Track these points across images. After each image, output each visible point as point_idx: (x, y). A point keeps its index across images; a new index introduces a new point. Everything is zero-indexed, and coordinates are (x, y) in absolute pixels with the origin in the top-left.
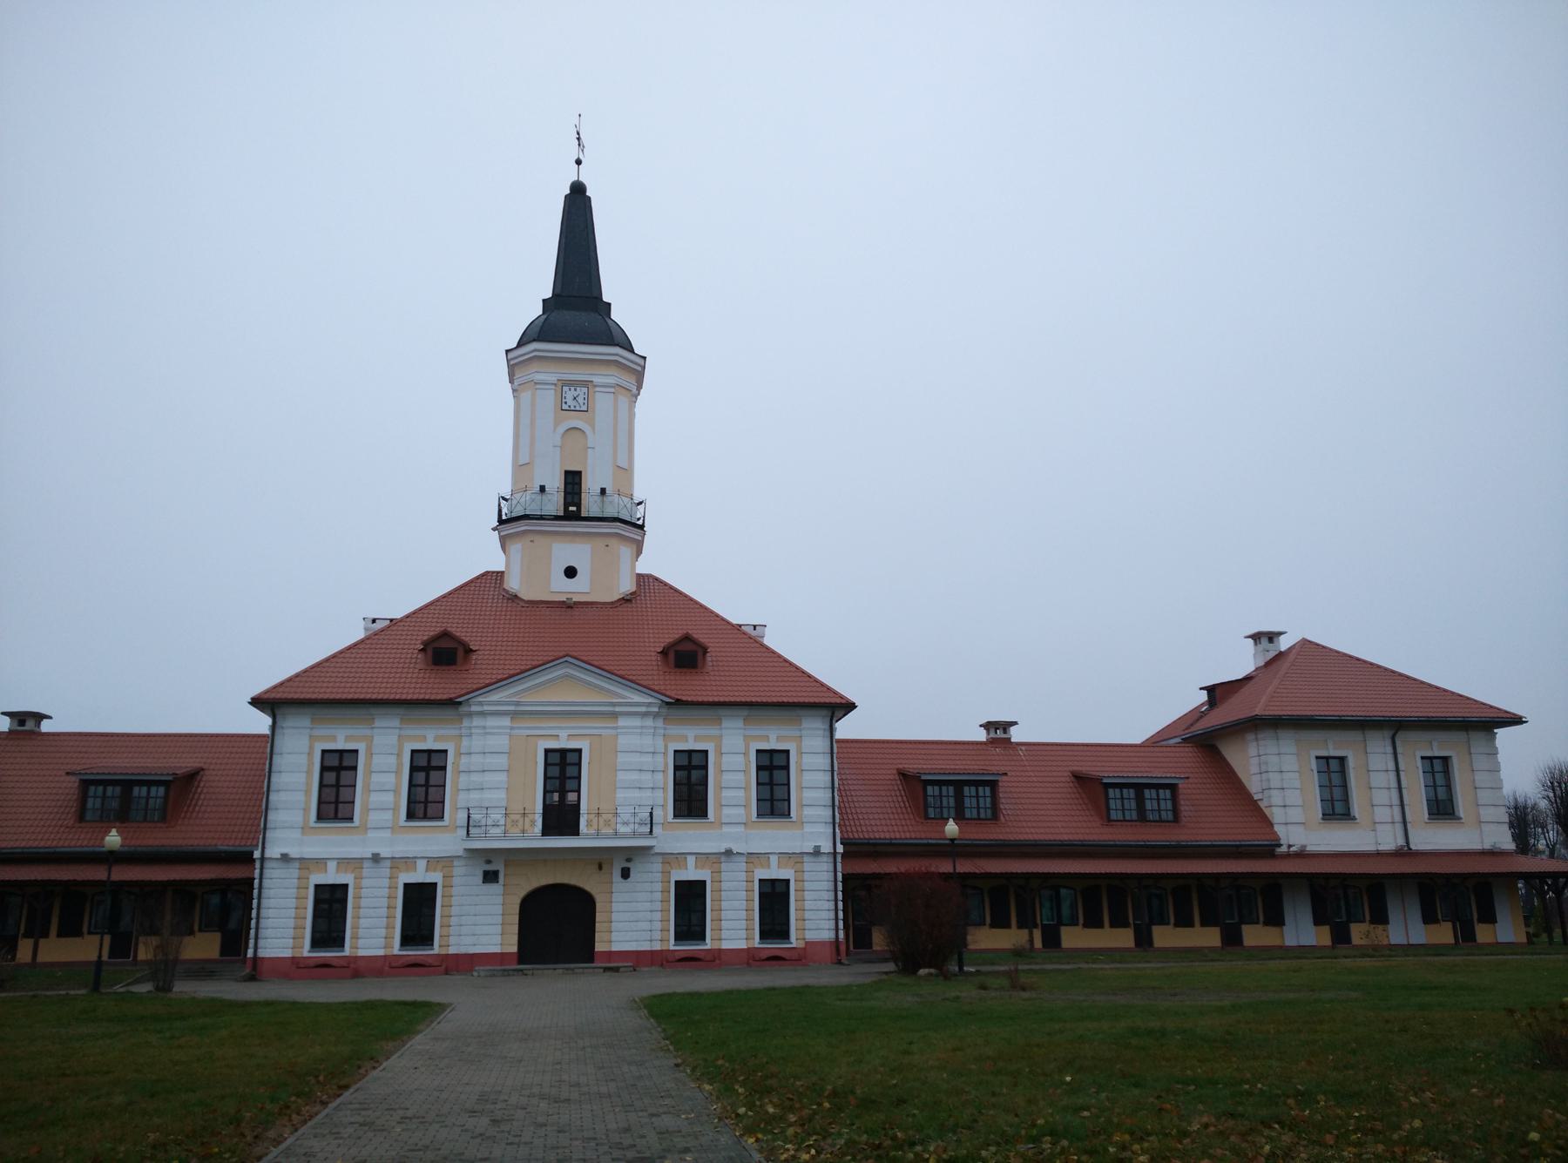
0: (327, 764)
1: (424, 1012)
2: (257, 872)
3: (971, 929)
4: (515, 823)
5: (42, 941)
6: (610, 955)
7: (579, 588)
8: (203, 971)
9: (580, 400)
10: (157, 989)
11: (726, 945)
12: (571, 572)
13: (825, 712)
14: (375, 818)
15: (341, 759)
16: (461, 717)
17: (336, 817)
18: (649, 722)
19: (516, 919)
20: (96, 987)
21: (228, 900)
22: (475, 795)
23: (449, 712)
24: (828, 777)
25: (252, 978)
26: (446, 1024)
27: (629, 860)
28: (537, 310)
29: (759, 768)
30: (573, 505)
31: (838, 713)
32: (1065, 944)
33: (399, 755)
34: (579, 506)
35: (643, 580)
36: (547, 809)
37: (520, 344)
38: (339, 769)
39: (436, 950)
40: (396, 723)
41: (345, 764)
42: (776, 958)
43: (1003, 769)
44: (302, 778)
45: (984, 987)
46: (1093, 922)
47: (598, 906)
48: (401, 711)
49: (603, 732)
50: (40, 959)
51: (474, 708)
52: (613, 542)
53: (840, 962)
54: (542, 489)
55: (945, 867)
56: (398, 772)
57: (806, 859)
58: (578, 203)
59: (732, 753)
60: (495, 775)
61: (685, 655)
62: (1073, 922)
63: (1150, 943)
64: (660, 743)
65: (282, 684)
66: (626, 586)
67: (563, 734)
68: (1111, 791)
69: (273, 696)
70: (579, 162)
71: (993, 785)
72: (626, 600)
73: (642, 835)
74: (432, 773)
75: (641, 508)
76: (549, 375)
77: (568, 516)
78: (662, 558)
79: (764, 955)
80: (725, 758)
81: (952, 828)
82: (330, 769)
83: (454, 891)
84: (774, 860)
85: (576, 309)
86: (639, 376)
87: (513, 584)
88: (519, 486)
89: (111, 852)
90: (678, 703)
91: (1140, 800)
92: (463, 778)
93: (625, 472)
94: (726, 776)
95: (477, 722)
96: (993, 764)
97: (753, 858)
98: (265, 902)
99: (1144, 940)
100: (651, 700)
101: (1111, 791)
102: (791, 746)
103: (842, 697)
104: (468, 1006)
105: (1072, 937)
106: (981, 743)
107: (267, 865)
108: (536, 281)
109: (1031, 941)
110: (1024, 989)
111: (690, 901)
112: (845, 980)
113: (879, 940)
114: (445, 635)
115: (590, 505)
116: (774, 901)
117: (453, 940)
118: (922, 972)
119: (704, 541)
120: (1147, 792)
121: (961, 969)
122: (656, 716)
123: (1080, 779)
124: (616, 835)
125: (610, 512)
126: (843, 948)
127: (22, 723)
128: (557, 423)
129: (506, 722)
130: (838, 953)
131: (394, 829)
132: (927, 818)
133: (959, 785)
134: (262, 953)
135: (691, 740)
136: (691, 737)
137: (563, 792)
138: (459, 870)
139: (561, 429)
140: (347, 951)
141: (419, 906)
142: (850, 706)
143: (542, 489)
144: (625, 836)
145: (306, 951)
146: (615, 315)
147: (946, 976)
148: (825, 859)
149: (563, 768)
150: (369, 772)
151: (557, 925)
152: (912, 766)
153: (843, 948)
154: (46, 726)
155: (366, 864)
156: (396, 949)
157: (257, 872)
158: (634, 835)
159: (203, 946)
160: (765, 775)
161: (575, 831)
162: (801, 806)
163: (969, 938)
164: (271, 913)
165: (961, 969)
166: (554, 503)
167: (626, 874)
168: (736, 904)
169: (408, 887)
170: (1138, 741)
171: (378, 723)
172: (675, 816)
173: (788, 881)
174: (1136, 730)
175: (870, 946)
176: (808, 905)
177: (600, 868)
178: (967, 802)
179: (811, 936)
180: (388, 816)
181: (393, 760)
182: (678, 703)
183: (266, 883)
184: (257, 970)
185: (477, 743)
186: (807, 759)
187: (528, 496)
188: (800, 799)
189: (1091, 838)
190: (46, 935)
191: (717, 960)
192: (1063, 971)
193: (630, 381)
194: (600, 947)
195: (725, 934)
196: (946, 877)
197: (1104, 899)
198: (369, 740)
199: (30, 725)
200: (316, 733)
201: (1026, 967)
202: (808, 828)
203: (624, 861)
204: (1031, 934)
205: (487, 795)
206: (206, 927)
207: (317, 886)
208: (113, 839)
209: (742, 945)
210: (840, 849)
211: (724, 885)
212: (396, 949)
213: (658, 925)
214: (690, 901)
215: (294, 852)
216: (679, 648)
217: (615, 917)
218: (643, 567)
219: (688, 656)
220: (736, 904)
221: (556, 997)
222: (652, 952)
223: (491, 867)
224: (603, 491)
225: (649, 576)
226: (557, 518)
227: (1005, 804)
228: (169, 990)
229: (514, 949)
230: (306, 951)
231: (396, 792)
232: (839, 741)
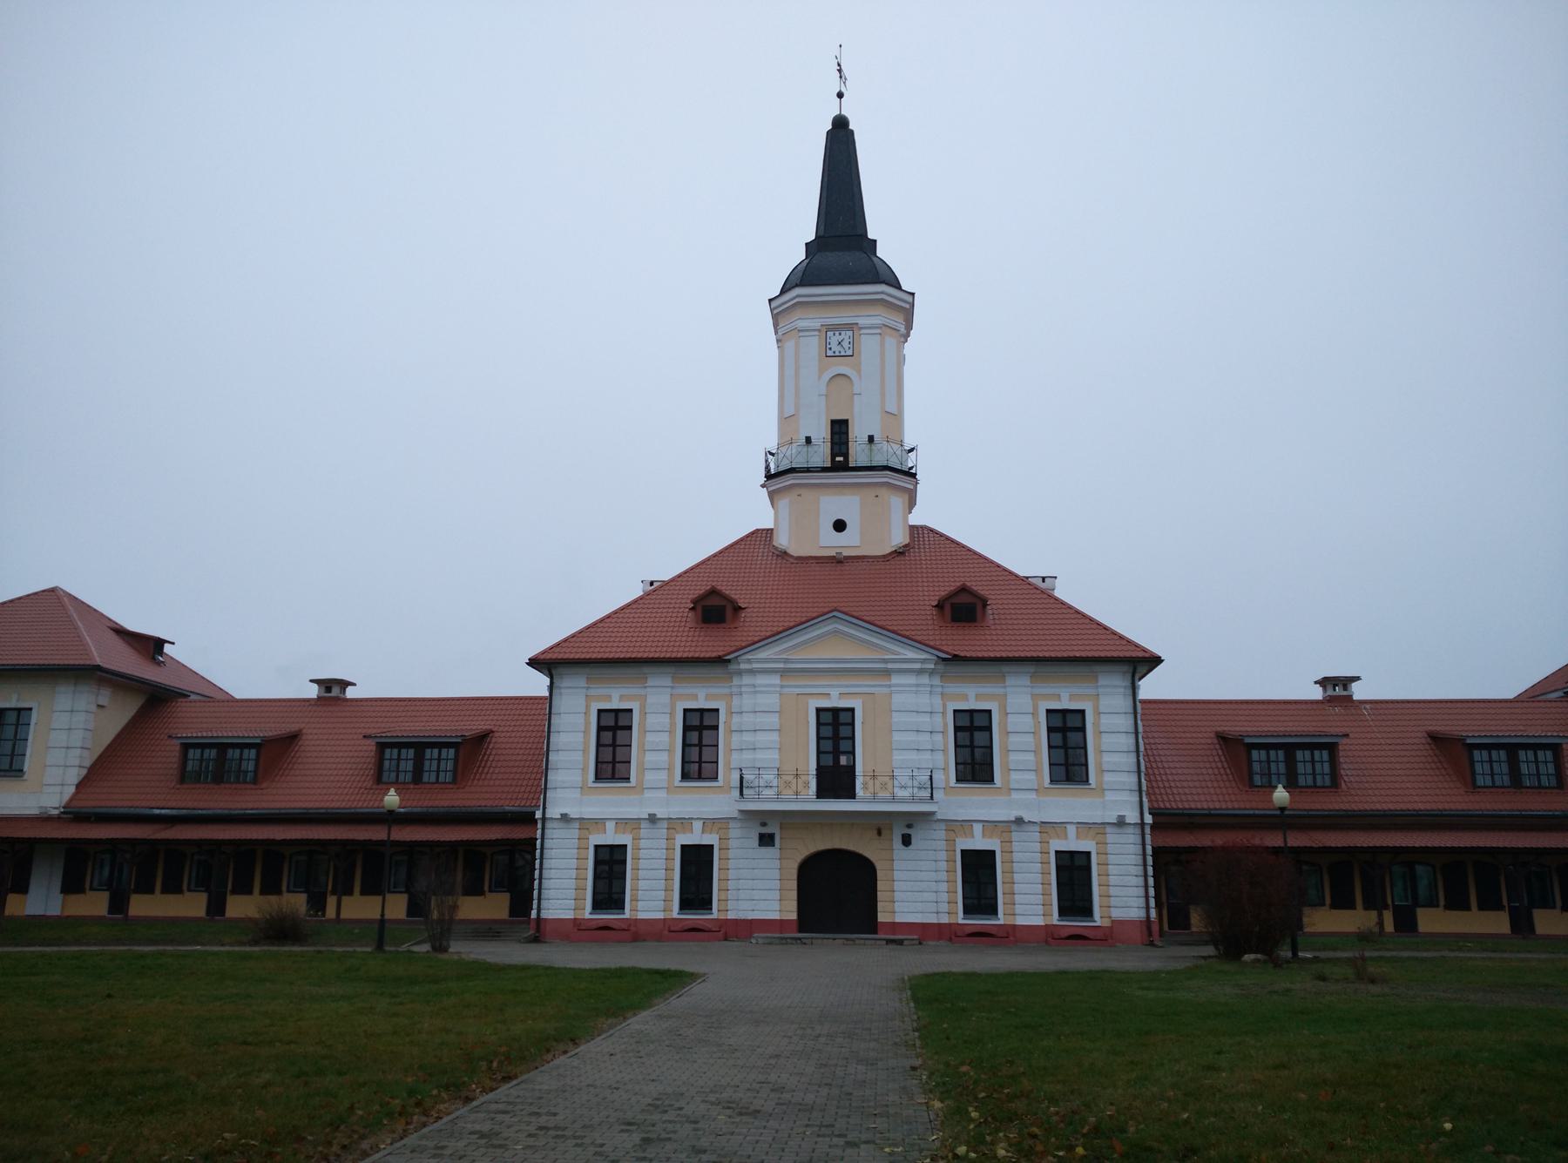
0: (603, 723)
1: (673, 980)
2: (539, 832)
3: (1306, 911)
4: (788, 784)
5: (345, 899)
6: (895, 926)
7: (849, 543)
8: (488, 931)
9: (845, 344)
10: (434, 949)
11: (1020, 921)
12: (840, 526)
13: (1125, 668)
14: (650, 777)
16: (730, 676)
17: (614, 777)
18: (925, 680)
19: (794, 884)
20: (380, 946)
21: (509, 862)
22: (747, 755)
23: (718, 671)
24: (1132, 740)
25: (536, 939)
26: (694, 995)
27: (909, 826)
28: (800, 255)
29: (1050, 730)
30: (840, 456)
31: (1141, 669)
32: (1539, 930)
33: (672, 714)
34: (846, 456)
35: (916, 531)
36: (821, 772)
37: (783, 291)
38: (615, 728)
39: (715, 915)
40: (667, 681)
41: (621, 723)
42: (695, 930)
43: (1347, 730)
44: (579, 737)
45: (1323, 978)
46: (1457, 902)
47: (880, 874)
48: (671, 669)
49: (872, 690)
50: (343, 916)
51: (743, 666)
52: (883, 492)
53: (1152, 944)
54: (808, 440)
55: (1274, 840)
56: (671, 732)
57: (1109, 829)
58: (840, 138)
59: (1020, 713)
60: (766, 732)
61: (963, 608)
62: (1432, 903)
63: (1532, 929)
64: (937, 701)
65: (558, 645)
66: (899, 538)
67: (835, 693)
68: (1476, 753)
69: (549, 656)
70: (840, 95)
71: (1332, 748)
72: (899, 553)
73: (921, 800)
74: (705, 733)
75: (912, 455)
76: (811, 320)
77: (836, 467)
78: (936, 508)
79: (1066, 933)
80: (1011, 718)
81: (1281, 795)
83: (731, 854)
84: (1071, 830)
85: (842, 248)
86: (908, 314)
87: (782, 541)
88: (786, 441)
89: (391, 812)
90: (956, 659)
91: (1513, 763)
92: (735, 738)
93: (895, 418)
94: (1013, 739)
95: (747, 680)
96: (1333, 723)
97: (1046, 827)
98: (546, 864)
99: (1522, 925)
100: (925, 656)
101: (1476, 753)
102: (1087, 706)
103: (1145, 650)
104: (721, 976)
105: (1431, 921)
106: (1317, 702)
107: (549, 825)
108: (801, 223)
109: (1381, 924)
110: (1373, 981)
111: (979, 873)
112: (1154, 965)
113: (1196, 920)
114: (713, 592)
115: (858, 453)
116: (1073, 875)
117: (730, 905)
118: (1248, 957)
119: (979, 491)
120: (1522, 754)
121: (1295, 954)
122: (932, 673)
123: (1436, 739)
124: (894, 799)
125: (879, 460)
126: (1155, 928)
127: (328, 690)
128: (821, 371)
129: (775, 680)
130: (1150, 934)
131: (670, 789)
132: (1252, 785)
133: (1290, 749)
134: (545, 914)
136: (972, 695)
137: (836, 753)
138: (735, 832)
140: (627, 914)
141: (697, 867)
142: (1155, 661)
143: (808, 440)
144: (903, 801)
145: (587, 913)
146: (811, 236)
147: (1277, 964)
148: (1131, 830)
149: (835, 728)
150: (644, 731)
151: (837, 892)
152: (1233, 727)
153: (1155, 928)
154: (351, 693)
155: (644, 825)
156: (675, 913)
157: (539, 832)
158: (913, 799)
159: (494, 906)
160: (1058, 738)
161: (850, 794)
162: (1101, 771)
163: (1305, 920)
164: (553, 873)
165: (1295, 954)
166: (821, 454)
167: (907, 841)
168: (654, 853)
169: (685, 849)
170: (1511, 696)
171: (651, 682)
172: (958, 780)
173: (1088, 854)
174: (1509, 686)
175: (1187, 926)
176: (1113, 880)
177: (879, 833)
178: (1301, 768)
179: (1117, 914)
180: (663, 775)
181: (666, 719)
182: (956, 659)
183: (548, 843)
184: (540, 932)
185: (747, 702)
186: (1105, 721)
187: (794, 449)
188: (1099, 764)
189: (1453, 806)
190: (350, 892)
191: (1011, 936)
192: (1423, 960)
193: (898, 321)
194: (882, 917)
195: (1018, 909)
196: (1276, 851)
197: (1467, 877)
198: (643, 699)
199: (335, 692)
200: (592, 692)
201: (1376, 954)
202: (1109, 796)
203: (905, 827)
204: (1380, 916)
205: (760, 755)
206: (496, 887)
207: (596, 847)
208: (392, 799)
209: (1039, 921)
210: (1148, 819)
211: (1017, 857)
212: (675, 913)
213: (945, 897)
214: (979, 873)
215: (573, 812)
216: (955, 600)
217: (897, 885)
218: (915, 519)
219: (967, 610)
220: (654, 853)
221: (845, 973)
222: (939, 925)
223: (768, 830)
224: (871, 439)
225: (923, 528)
226: (824, 470)
227: (1347, 769)
228: (445, 950)
229: (794, 916)
230: (587, 913)
231: (670, 751)
232: (1144, 702)
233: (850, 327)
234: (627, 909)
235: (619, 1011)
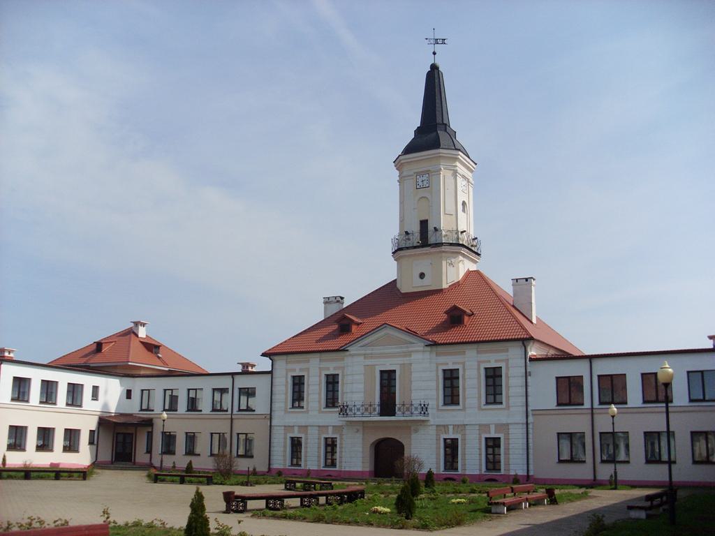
15: (494, 372)
30: (422, 239)
58: (434, 79)
59: (471, 367)
69: (271, 352)
70: (434, 53)
79: (445, 477)
82: (491, 377)
90: (435, 344)
135: (331, 369)
136: (450, 361)
141: (331, 445)
149: (388, 378)
161: (393, 414)
166: (416, 239)
198: (308, 370)
233: (428, 172)
234: (337, 466)
235: (202, 508)
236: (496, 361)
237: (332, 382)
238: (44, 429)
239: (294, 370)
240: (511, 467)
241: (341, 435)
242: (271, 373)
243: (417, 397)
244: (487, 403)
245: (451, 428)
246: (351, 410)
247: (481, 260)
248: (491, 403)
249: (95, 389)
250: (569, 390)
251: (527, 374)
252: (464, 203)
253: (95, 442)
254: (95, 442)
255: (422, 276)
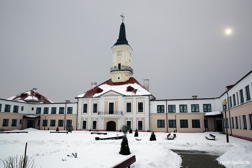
19: (110, 132)
58: (123, 26)
70: (123, 20)
139: (118, 57)
149: (111, 105)
159: (163, 107)
198: (99, 102)
236: (141, 101)
237: (95, 106)
238: (14, 120)
239: (94, 102)
240: (145, 129)
241: (98, 120)
242: (77, 103)
243: (120, 110)
244: (139, 112)
245: (129, 118)
246: (120, 113)
247: (133, 75)
248: (140, 112)
249: (22, 107)
250: (160, 109)
251: (150, 104)
252: (130, 60)
253: (22, 123)
254: (22, 123)
255: (119, 78)
